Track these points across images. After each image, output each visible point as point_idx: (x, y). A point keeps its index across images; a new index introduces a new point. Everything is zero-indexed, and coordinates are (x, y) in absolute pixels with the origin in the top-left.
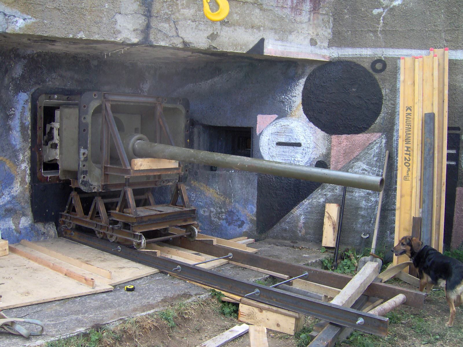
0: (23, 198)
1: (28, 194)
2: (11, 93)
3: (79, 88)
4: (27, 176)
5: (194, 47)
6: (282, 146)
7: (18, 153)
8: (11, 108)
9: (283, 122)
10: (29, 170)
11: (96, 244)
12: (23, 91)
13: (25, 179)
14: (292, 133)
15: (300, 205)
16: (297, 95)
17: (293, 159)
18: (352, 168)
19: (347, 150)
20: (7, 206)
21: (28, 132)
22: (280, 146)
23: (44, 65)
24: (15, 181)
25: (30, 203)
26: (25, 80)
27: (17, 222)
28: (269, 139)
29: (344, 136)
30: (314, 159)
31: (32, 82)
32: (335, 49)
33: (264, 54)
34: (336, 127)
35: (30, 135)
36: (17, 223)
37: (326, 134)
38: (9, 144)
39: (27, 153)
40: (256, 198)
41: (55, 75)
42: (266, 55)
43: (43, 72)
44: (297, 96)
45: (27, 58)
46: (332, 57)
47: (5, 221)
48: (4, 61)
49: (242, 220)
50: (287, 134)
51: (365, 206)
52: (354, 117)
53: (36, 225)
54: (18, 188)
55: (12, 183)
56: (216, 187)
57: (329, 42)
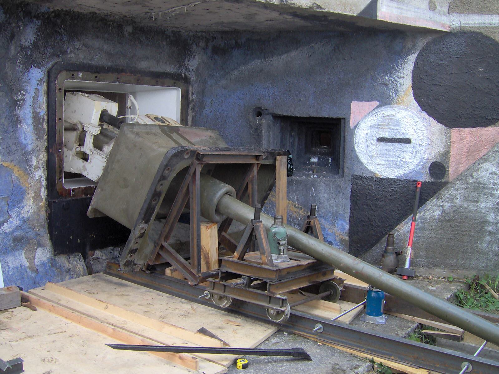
0: (38, 220)
1: (43, 214)
2: (19, 69)
3: (110, 64)
4: (43, 189)
5: (294, 4)
6: (385, 143)
7: (30, 157)
8: (20, 91)
9: (387, 111)
10: (45, 181)
11: (164, 285)
12: (36, 65)
13: (40, 194)
14: (399, 125)
15: (408, 220)
16: (405, 75)
17: (399, 159)
18: (477, 171)
19: (472, 148)
20: (15, 234)
21: (43, 126)
22: (382, 143)
23: (64, 29)
24: (26, 197)
25: (47, 228)
26: (38, 51)
27: (31, 257)
28: (367, 134)
29: (468, 130)
30: (428, 159)
31: (48, 54)
32: (456, 16)
33: (378, 19)
34: (457, 117)
35: (46, 129)
36: (32, 258)
37: (444, 127)
38: (18, 143)
39: (42, 156)
40: (349, 211)
41: (78, 45)
42: (379, 19)
43: (63, 39)
44: (405, 76)
45: (41, 17)
46: (453, 26)
47: (14, 255)
48: (9, 21)
49: (329, 240)
50: (392, 127)
51: (494, 219)
52: (481, 105)
53: (57, 259)
54: (30, 207)
55: (22, 201)
56: (294, 198)
57: (449, 7)
